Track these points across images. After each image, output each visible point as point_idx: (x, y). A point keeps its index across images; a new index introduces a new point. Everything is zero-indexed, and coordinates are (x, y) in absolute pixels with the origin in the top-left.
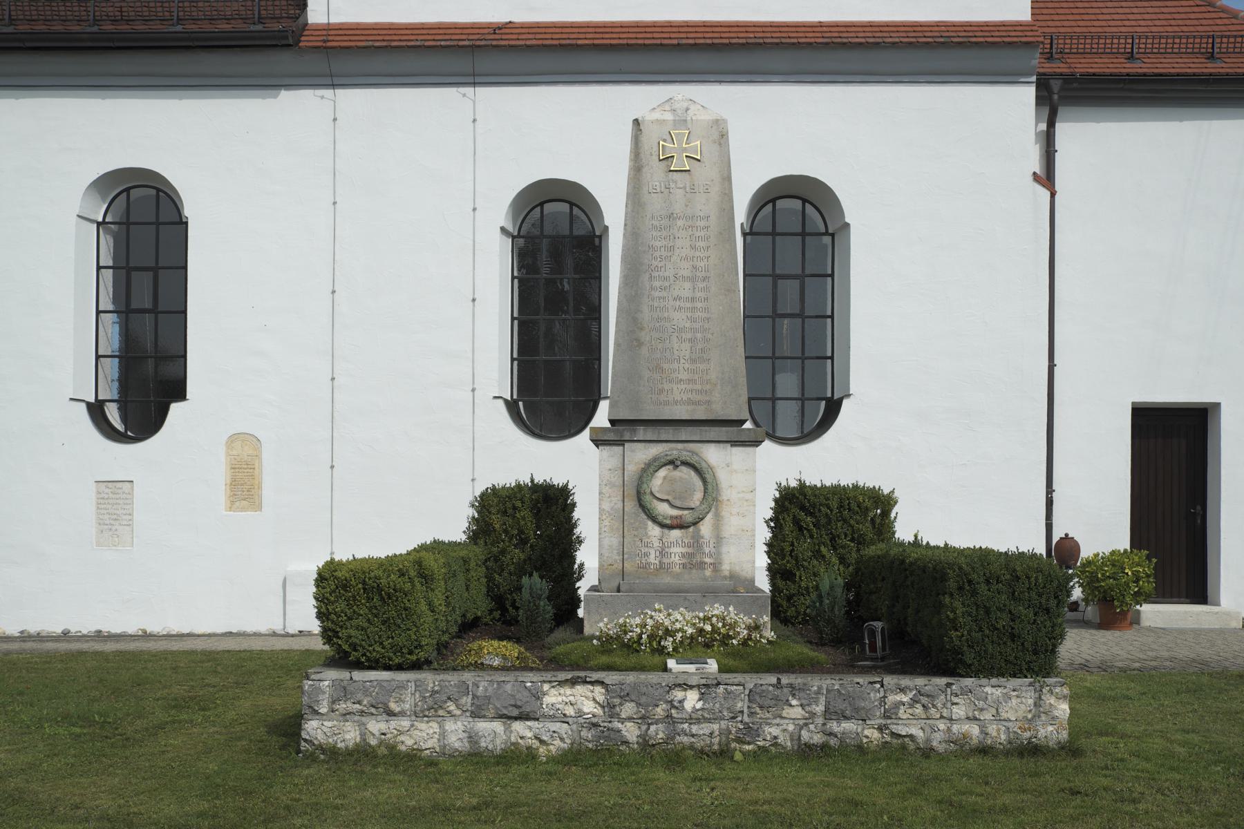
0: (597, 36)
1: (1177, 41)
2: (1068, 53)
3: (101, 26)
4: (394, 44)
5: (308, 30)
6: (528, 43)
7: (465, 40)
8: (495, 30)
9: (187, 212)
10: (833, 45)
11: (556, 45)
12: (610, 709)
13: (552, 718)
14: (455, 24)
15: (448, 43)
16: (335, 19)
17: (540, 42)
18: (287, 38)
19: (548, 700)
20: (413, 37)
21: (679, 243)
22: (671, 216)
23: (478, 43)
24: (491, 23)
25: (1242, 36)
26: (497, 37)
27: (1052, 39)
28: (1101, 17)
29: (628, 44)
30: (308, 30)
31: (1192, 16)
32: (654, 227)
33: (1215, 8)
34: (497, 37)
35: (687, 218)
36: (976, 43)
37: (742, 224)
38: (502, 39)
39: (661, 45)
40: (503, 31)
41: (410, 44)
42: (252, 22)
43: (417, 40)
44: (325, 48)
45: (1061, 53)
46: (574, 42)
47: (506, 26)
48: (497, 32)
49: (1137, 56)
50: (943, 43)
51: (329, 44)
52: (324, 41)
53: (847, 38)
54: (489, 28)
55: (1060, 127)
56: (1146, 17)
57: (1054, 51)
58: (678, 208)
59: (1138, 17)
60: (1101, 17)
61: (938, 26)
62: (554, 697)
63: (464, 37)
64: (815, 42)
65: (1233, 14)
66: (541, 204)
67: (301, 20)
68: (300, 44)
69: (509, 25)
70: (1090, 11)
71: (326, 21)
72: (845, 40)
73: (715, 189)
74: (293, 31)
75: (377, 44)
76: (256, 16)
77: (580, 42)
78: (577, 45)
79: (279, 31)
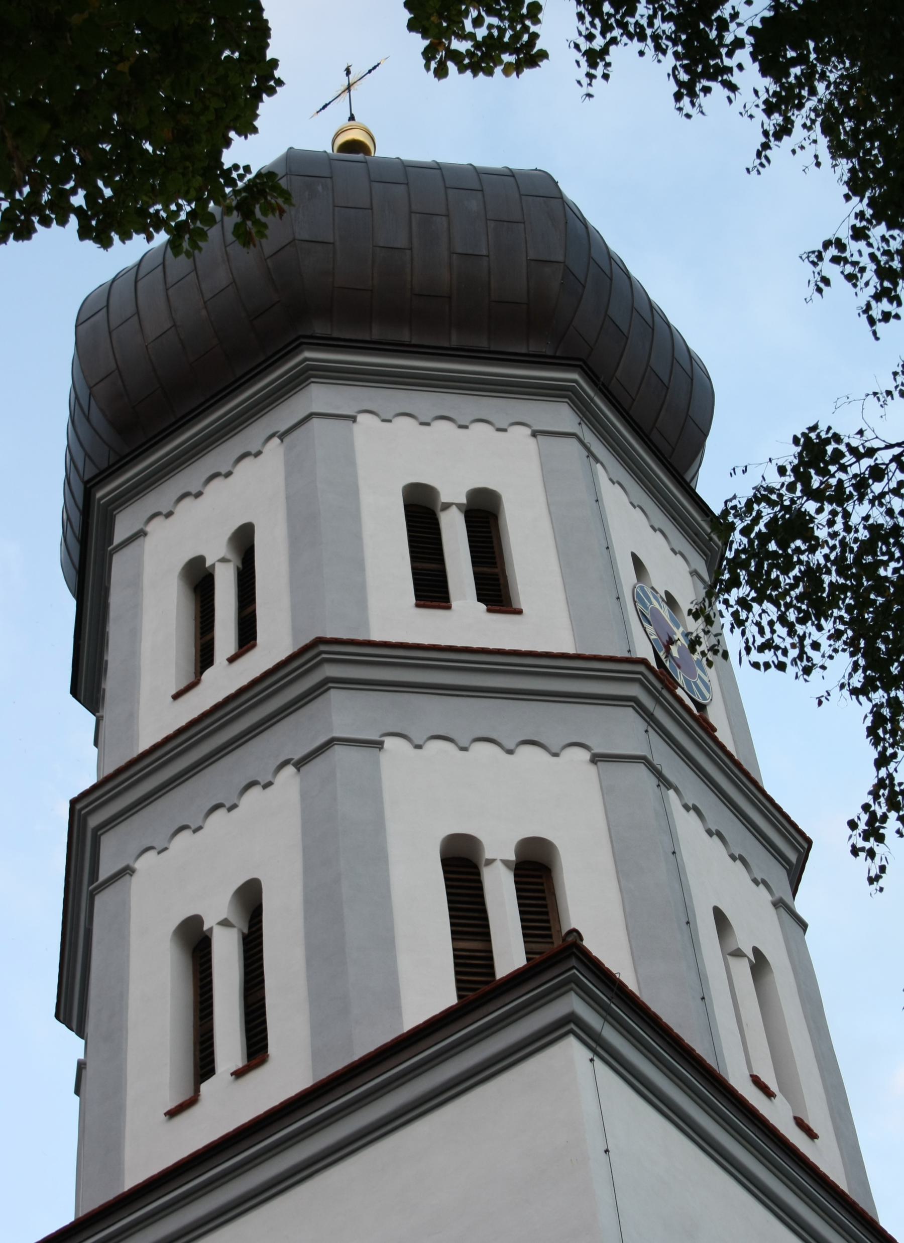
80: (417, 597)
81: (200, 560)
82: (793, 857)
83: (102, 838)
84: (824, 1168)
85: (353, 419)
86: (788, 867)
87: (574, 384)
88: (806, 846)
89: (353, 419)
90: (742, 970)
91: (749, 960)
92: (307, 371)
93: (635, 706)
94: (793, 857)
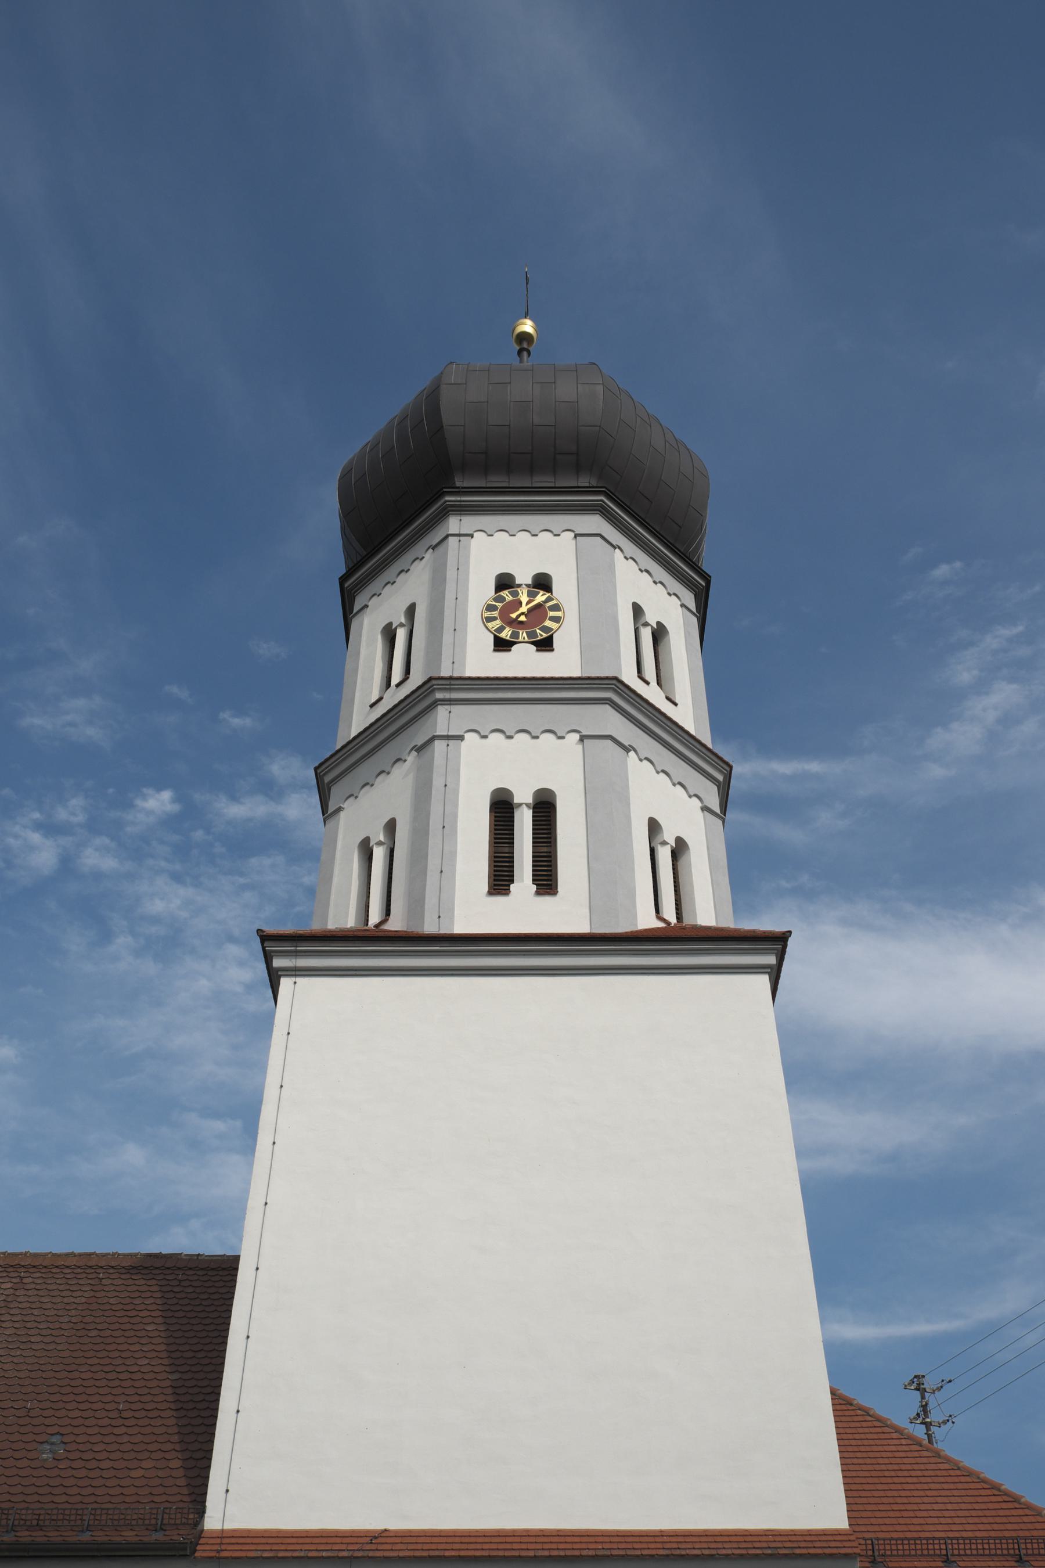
2: (889, 1556)
3: (17, 1531)
4: (281, 1554)
5: (203, 1537)
6: (401, 1554)
7: (344, 1550)
8: (371, 1540)
10: (672, 1557)
11: (424, 1557)
14: (337, 1531)
15: (329, 1554)
16: (228, 1526)
17: (411, 1554)
18: (185, 1549)
20: (298, 1547)
23: (356, 1554)
24: (368, 1531)
25: (1044, 1539)
26: (373, 1547)
27: (872, 1544)
28: (919, 1514)
29: (489, 1556)
30: (203, 1537)
31: (1001, 1513)
33: (1020, 1504)
34: (373, 1547)
36: (801, 1555)
37: (944, 1451)
38: (377, 1550)
39: (520, 1557)
42: (154, 1529)
43: (301, 1550)
44: (219, 1558)
45: (883, 1555)
46: (441, 1553)
47: (382, 1535)
48: (373, 1541)
49: (953, 1559)
50: (770, 1555)
52: (218, 1551)
53: (685, 1549)
54: (366, 1536)
56: (960, 1513)
57: (876, 1553)
59: (952, 1514)
60: (919, 1514)
61: (766, 1535)
63: (344, 1547)
64: (657, 1555)
65: (1038, 1512)
67: (199, 1528)
68: (196, 1555)
70: (909, 1507)
71: (220, 1528)
72: (683, 1552)
74: (191, 1542)
75: (265, 1554)
76: (159, 1523)
77: (447, 1554)
78: (445, 1557)
79: (180, 1543)
80: (495, 646)
81: (390, 624)
82: (720, 778)
83: (332, 788)
84: (687, 728)
85: (472, 536)
86: (717, 784)
87: (601, 502)
88: (728, 769)
89: (472, 536)
90: (646, 635)
91: (652, 627)
92: (437, 702)
93: (601, 509)
94: (720, 778)
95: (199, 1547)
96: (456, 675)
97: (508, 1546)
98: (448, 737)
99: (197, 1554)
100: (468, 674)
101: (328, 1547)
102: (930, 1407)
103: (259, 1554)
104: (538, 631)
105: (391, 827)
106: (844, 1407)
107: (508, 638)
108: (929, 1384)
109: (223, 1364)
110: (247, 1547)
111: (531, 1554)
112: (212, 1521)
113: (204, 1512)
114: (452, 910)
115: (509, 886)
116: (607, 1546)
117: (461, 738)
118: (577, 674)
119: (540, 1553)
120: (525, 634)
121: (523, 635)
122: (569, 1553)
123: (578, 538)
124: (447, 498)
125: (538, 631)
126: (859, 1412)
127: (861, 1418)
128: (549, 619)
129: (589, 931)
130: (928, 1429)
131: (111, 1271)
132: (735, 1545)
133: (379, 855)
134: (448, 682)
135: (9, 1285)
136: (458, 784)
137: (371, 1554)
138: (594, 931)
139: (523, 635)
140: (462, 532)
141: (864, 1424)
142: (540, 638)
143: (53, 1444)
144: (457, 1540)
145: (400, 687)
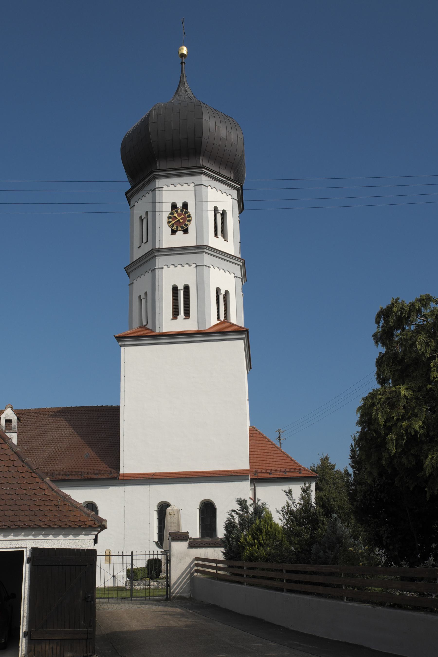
0: (171, 476)
1: (279, 471)
4: (135, 478)
6: (159, 478)
9: (98, 509)
12: (158, 584)
13: (152, 585)
16: (125, 473)
19: (152, 583)
20: (139, 477)
21: (172, 526)
22: (171, 522)
24: (152, 473)
32: (169, 524)
35: (173, 522)
40: (155, 475)
41: (138, 478)
51: (124, 479)
55: (256, 488)
58: (172, 521)
62: (152, 583)
66: (162, 505)
69: (156, 473)
73: (177, 518)
78: (167, 478)
95: (119, 478)
96: (161, 247)
97: (180, 475)
98: (159, 268)
99: (119, 479)
100: (164, 247)
101: (145, 477)
102: (281, 436)
103: (131, 478)
104: (184, 226)
105: (146, 293)
106: (261, 437)
107: (175, 229)
108: (281, 431)
109: (120, 413)
110: (129, 477)
111: (184, 477)
112: (121, 472)
113: (120, 470)
114: (162, 325)
115: (177, 316)
116: (199, 475)
117: (162, 268)
118: (195, 244)
119: (186, 477)
120: (180, 227)
121: (180, 228)
122: (192, 476)
123: (196, 186)
124: (155, 173)
125: (184, 226)
126: (264, 438)
127: (264, 440)
128: (187, 221)
129: (197, 329)
130: (280, 441)
131: (92, 411)
132: (225, 474)
133: (144, 301)
134: (158, 250)
135: (69, 416)
136: (162, 284)
137: (153, 478)
138: (200, 329)
139: (180, 228)
140: (160, 187)
141: (265, 441)
142: (184, 228)
143: (87, 455)
144: (170, 474)
145: (146, 244)
